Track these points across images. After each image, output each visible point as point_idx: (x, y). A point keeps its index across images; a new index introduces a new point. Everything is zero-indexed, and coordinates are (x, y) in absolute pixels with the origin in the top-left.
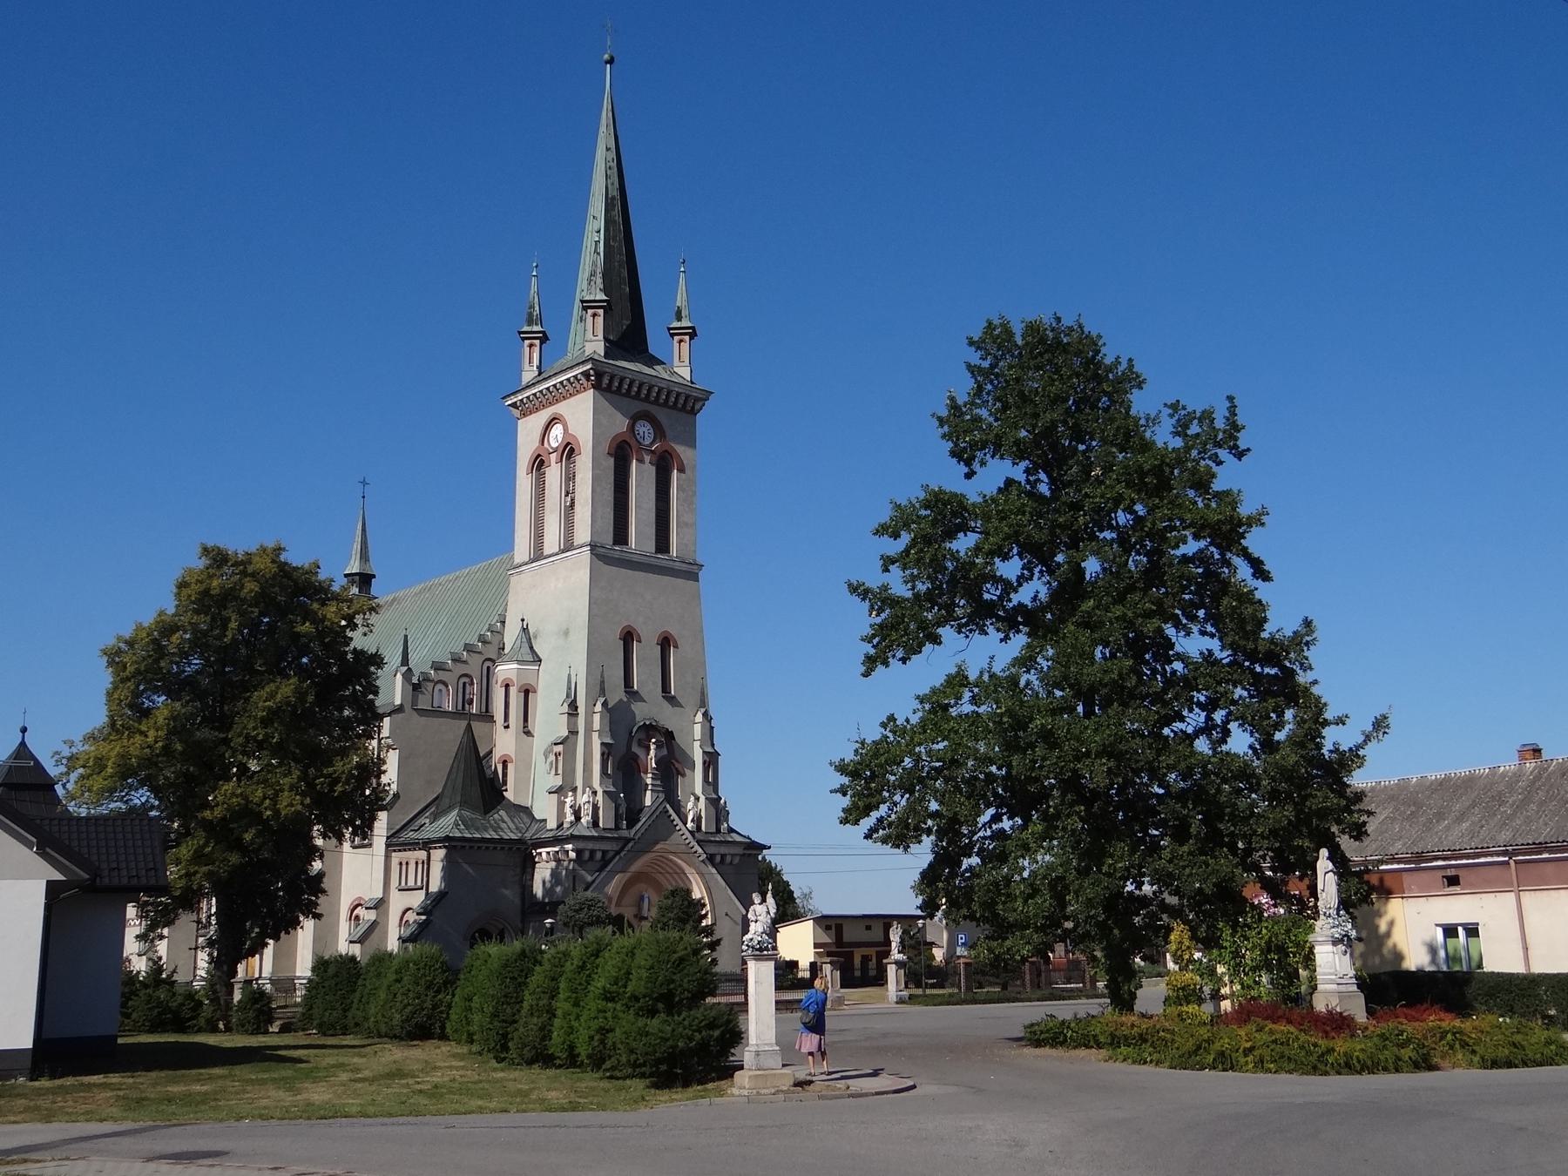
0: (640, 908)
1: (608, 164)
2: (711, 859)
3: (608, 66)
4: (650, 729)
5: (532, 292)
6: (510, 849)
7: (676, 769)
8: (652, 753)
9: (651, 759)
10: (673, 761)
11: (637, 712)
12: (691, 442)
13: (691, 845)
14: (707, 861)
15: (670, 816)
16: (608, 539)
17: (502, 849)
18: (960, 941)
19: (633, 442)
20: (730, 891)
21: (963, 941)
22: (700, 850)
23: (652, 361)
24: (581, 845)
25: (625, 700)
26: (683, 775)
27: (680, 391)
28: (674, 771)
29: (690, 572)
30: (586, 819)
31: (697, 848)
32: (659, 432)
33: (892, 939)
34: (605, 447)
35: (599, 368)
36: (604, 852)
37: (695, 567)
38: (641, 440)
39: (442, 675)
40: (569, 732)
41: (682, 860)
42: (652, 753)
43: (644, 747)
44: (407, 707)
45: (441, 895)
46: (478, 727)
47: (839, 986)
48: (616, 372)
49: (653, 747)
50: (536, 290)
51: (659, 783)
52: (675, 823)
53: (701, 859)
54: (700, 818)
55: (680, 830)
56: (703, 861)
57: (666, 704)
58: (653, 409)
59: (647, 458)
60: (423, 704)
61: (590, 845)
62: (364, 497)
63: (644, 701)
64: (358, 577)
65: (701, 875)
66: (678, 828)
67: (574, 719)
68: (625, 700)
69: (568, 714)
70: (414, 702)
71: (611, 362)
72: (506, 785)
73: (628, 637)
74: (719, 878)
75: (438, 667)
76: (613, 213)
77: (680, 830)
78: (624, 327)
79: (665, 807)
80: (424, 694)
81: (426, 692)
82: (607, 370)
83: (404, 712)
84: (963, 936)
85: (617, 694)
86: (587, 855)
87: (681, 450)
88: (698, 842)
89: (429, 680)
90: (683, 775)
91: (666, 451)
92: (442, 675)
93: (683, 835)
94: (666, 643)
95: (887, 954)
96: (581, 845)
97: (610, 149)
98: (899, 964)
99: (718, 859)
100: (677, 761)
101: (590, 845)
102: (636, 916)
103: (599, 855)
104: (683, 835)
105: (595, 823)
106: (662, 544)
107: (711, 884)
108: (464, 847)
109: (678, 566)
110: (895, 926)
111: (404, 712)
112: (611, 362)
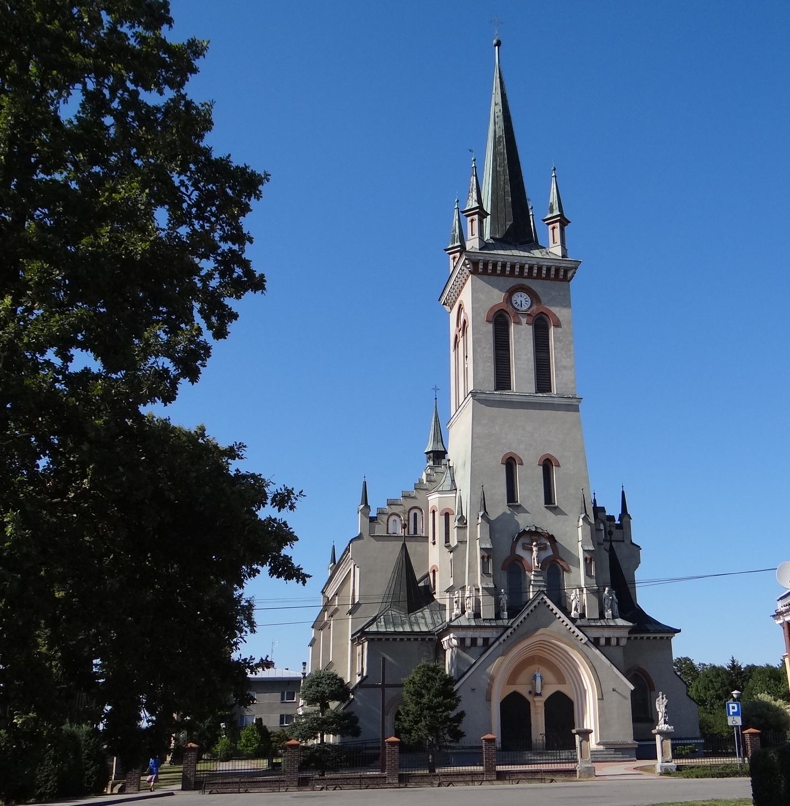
0: (534, 686)
1: (496, 115)
2: (596, 642)
3: (497, 47)
4: (535, 534)
5: (455, 220)
6: (423, 640)
7: (562, 566)
8: (535, 554)
9: (534, 559)
10: (559, 561)
11: (520, 522)
12: (566, 303)
13: (572, 630)
14: (589, 643)
15: (549, 606)
16: (490, 384)
17: (416, 639)
18: (731, 711)
19: (509, 309)
20: (615, 670)
21: (736, 710)
22: (581, 634)
23: (537, 246)
24: (462, 634)
25: (509, 512)
26: (569, 571)
27: (550, 264)
28: (561, 568)
29: (571, 406)
30: (469, 612)
31: (577, 631)
32: (535, 297)
33: (658, 710)
34: (484, 316)
35: (473, 258)
36: (486, 640)
37: (574, 400)
38: (519, 308)
39: (395, 509)
40: (458, 541)
41: (565, 644)
42: (535, 554)
43: (529, 550)
44: (366, 535)
45: (367, 676)
46: (411, 546)
47: (671, 756)
48: (488, 259)
49: (535, 549)
50: (457, 218)
51: (541, 578)
52: (554, 612)
53: (583, 641)
54: (584, 606)
55: (560, 618)
56: (585, 643)
57: (549, 514)
58: (528, 282)
59: (524, 320)
60: (380, 530)
61: (470, 634)
62: (436, 399)
63: (528, 512)
64: (432, 454)
65: (586, 657)
66: (558, 616)
67: (462, 531)
68: (509, 512)
69: (458, 527)
70: (371, 530)
71: (492, 252)
72: (435, 589)
73: (510, 463)
74: (603, 658)
75: (391, 503)
76: (499, 148)
77: (560, 618)
78: (508, 227)
79: (543, 598)
80: (380, 524)
81: (381, 523)
82: (480, 258)
83: (363, 539)
84: (735, 705)
85: (499, 507)
86: (468, 642)
87: (558, 311)
88: (578, 627)
89: (383, 513)
90: (569, 571)
91: (542, 313)
92: (395, 509)
93: (563, 621)
94: (547, 465)
95: (654, 722)
96: (462, 634)
97: (498, 104)
98: (665, 735)
99: (603, 642)
100: (563, 560)
101: (470, 634)
102: (530, 692)
103: (480, 642)
104: (563, 621)
105: (477, 615)
106: (543, 382)
107: (596, 664)
108: (381, 639)
109: (557, 401)
110: (660, 697)
111: (363, 539)
112: (492, 252)
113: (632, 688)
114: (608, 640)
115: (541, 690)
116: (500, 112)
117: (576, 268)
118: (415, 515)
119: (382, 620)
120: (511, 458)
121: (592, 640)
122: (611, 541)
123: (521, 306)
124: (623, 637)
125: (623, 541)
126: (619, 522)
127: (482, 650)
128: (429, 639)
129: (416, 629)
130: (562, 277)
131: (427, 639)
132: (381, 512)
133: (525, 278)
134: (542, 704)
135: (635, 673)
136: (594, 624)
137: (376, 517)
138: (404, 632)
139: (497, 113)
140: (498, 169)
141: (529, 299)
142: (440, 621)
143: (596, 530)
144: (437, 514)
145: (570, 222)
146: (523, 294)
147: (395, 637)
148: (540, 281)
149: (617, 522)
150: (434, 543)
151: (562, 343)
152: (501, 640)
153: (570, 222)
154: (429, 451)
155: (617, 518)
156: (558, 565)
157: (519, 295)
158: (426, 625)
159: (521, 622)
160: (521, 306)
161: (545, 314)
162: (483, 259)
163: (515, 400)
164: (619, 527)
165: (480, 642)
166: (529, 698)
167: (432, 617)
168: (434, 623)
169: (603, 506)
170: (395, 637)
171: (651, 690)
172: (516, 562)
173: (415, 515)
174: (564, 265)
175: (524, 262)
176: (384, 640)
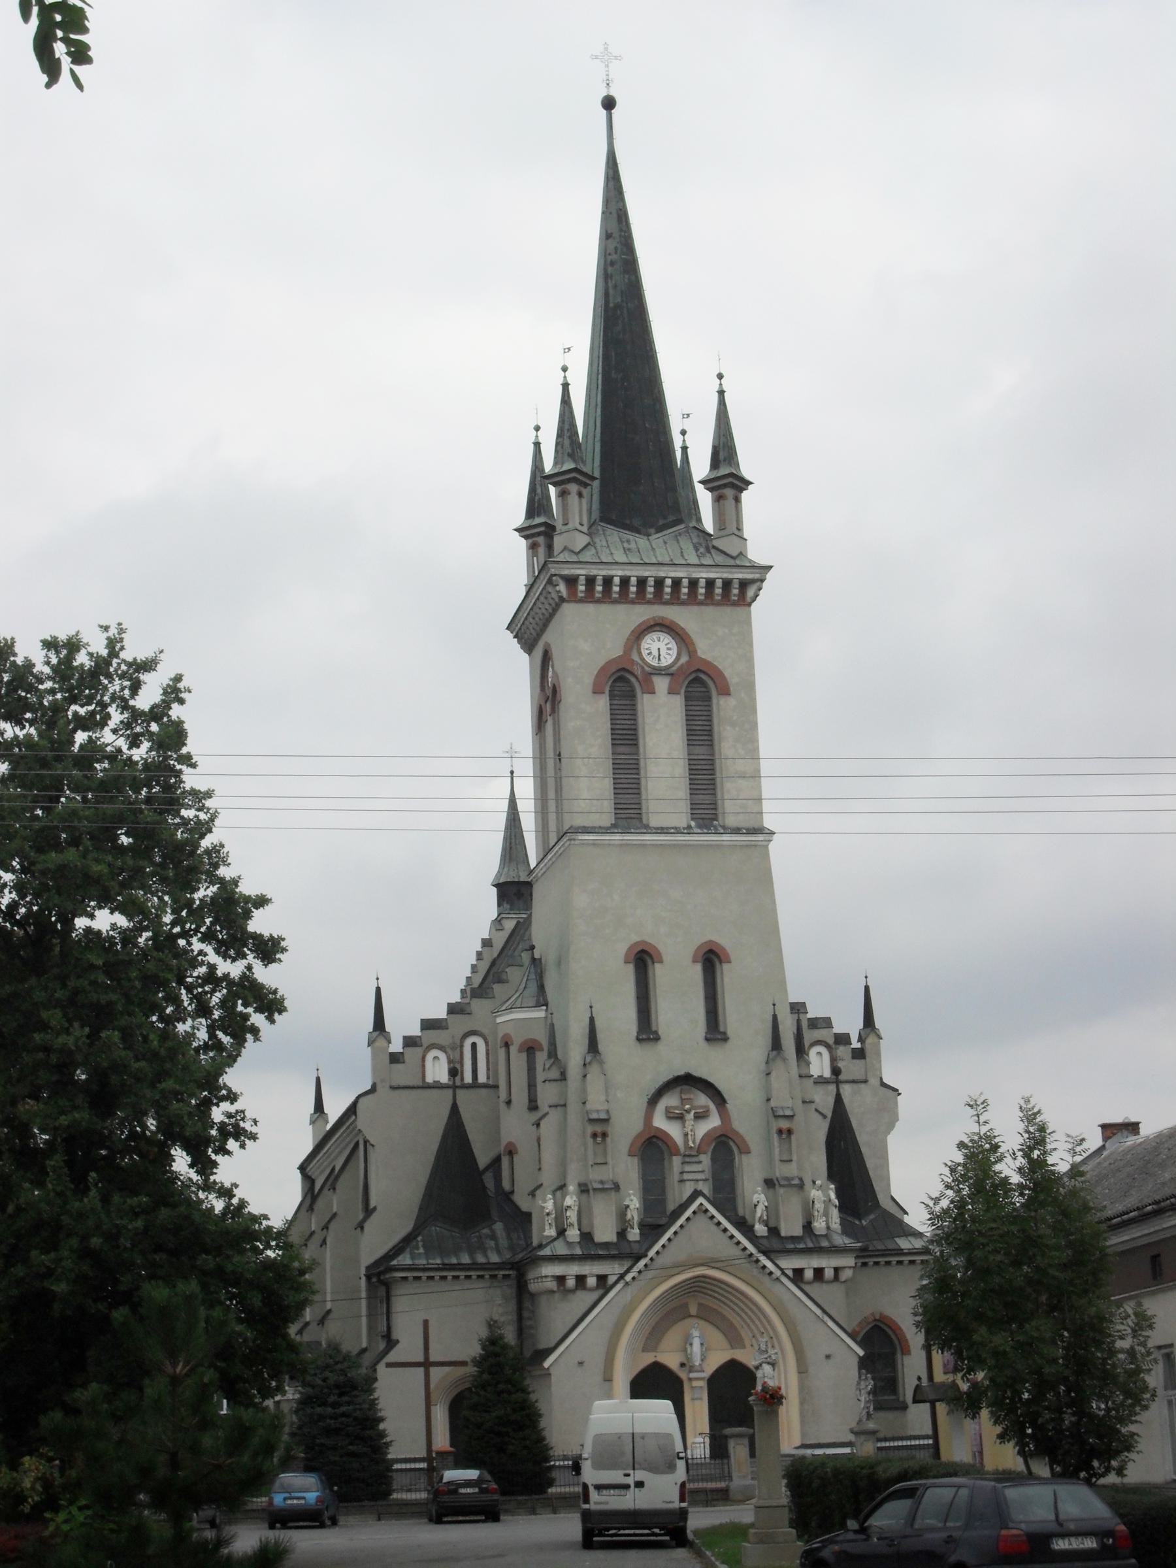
30: (573, 1234)
36: (602, 1279)
75: (427, 1025)
102: (682, 1365)
103: (591, 1282)
105: (586, 1237)
113: (861, 1353)
114: (819, 1272)
115: (702, 1360)
116: (616, 253)
117: (762, 581)
118: (474, 1045)
119: (420, 1244)
120: (643, 951)
121: (790, 1273)
122: (838, 1083)
123: (659, 659)
124: (844, 1268)
125: (865, 1081)
126: (859, 1045)
127: (595, 1296)
128: (503, 1275)
129: (481, 1259)
130: (736, 598)
131: (500, 1276)
132: (409, 1042)
133: (666, 603)
134: (703, 1384)
135: (875, 1325)
136: (792, 1246)
137: (402, 1053)
138: (459, 1264)
139: (610, 254)
140: (613, 375)
141: (673, 645)
142: (522, 1242)
143: (800, 1076)
144: (513, 1049)
145: (751, 483)
146: (662, 635)
147: (444, 1274)
148: (695, 608)
149: (856, 1044)
150: (509, 1103)
151: (737, 729)
152: (628, 1278)
153: (751, 483)
154: (501, 882)
155: (854, 1038)
156: (731, 1143)
157: (655, 637)
158: (499, 1252)
159: (663, 1246)
160: (659, 659)
161: (704, 672)
162: (584, 573)
163: (648, 843)
164: (859, 1054)
165: (591, 1282)
166: (683, 1375)
167: (509, 1238)
168: (512, 1248)
169: (828, 1016)
170: (444, 1274)
171: (903, 1354)
172: (655, 1140)
173: (474, 1045)
174: (740, 576)
175: (663, 575)
176: (424, 1278)
